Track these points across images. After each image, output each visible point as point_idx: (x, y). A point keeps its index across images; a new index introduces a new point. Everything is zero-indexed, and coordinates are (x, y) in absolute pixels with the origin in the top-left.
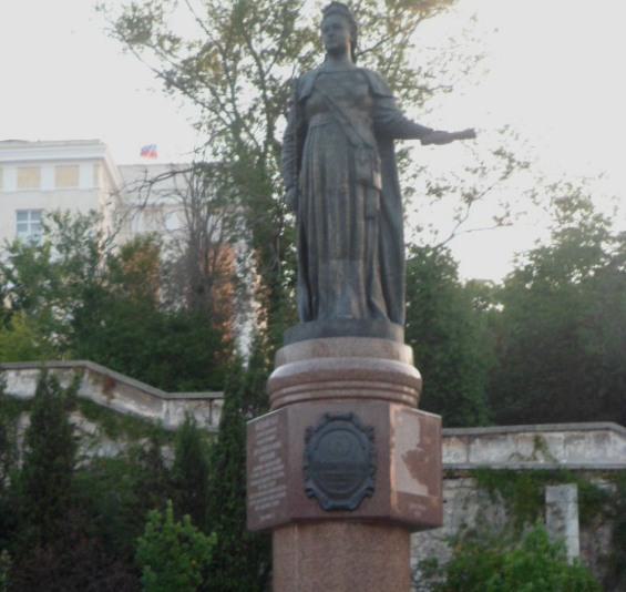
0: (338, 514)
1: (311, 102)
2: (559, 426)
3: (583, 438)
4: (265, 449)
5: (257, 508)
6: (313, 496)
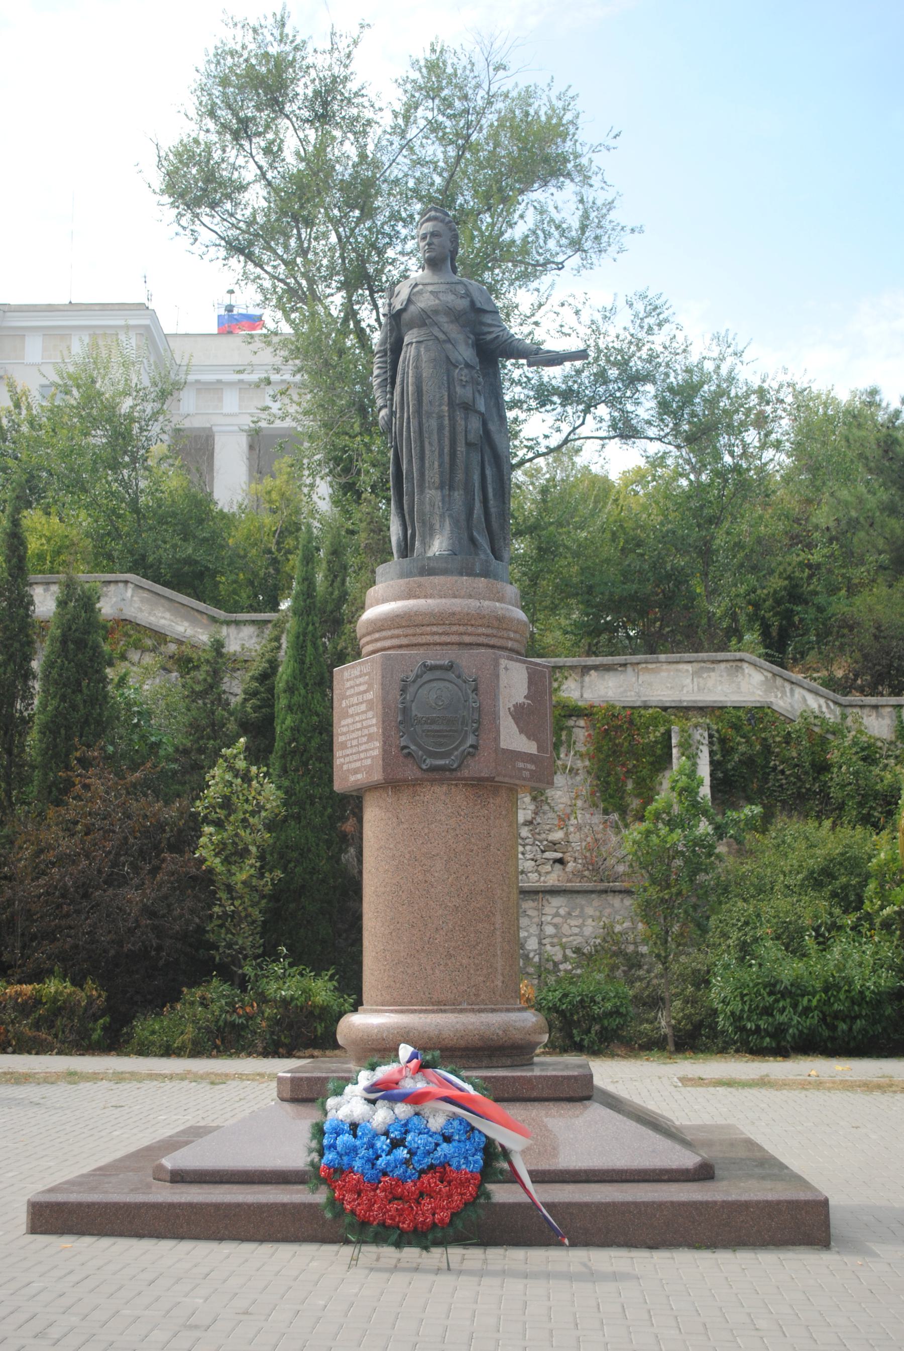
0: (440, 774)
1: (406, 316)
3: (713, 670)
4: (355, 700)
5: (345, 767)
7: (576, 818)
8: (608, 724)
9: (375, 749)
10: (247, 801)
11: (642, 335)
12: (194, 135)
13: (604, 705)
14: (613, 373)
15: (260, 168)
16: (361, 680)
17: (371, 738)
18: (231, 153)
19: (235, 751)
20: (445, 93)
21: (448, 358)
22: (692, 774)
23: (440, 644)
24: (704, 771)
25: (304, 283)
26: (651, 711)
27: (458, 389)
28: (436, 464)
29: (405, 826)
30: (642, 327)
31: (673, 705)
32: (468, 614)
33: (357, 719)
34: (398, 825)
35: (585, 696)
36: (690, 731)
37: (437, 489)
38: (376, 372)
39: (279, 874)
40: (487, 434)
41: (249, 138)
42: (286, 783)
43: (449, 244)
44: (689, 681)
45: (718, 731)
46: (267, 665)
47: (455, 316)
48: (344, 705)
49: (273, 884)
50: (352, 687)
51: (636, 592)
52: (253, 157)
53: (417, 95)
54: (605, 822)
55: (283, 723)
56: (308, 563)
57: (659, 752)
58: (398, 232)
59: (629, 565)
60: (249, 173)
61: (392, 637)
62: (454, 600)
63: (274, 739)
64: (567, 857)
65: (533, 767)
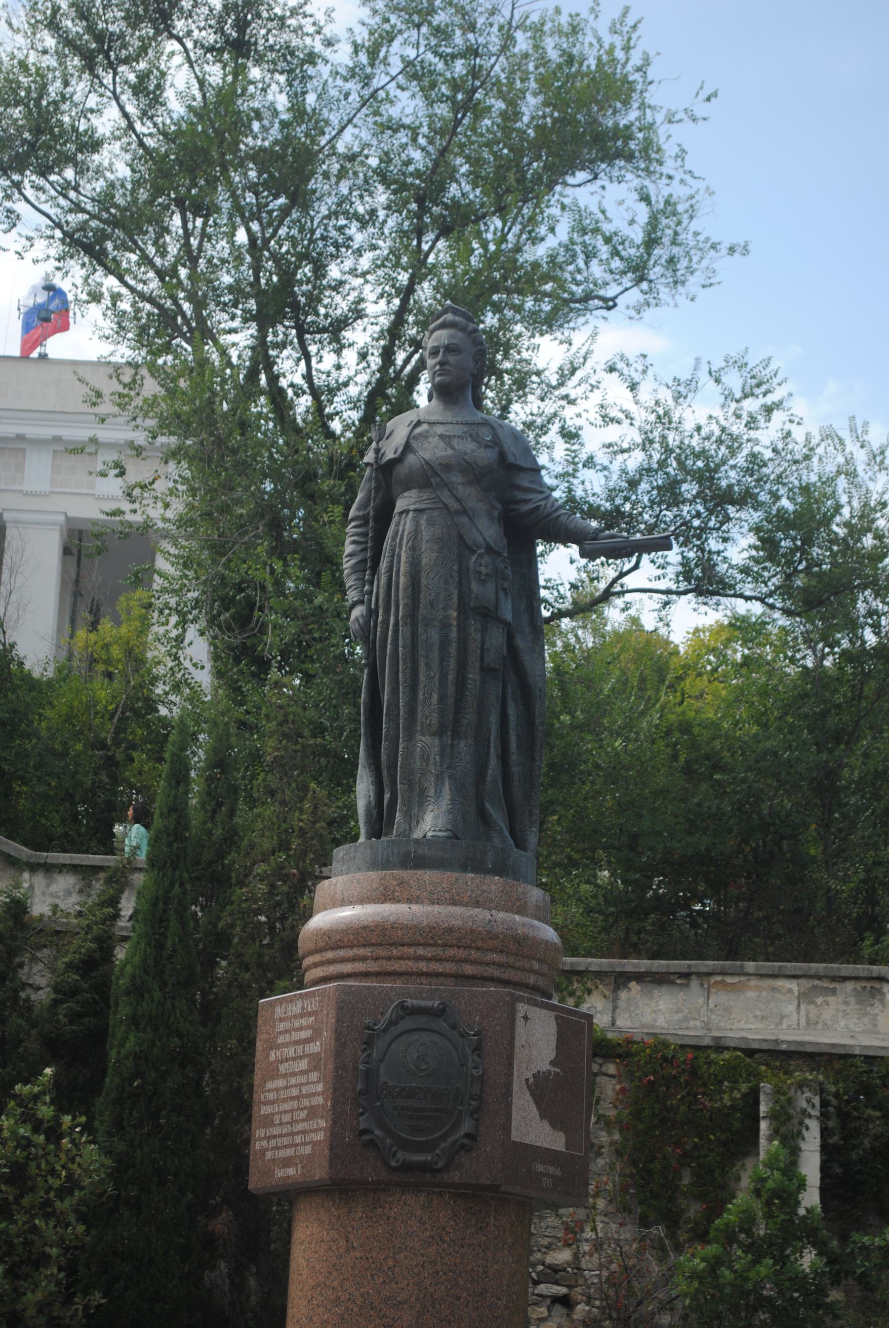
0: (416, 1178)
1: (402, 470)
2: (790, 967)
3: (834, 992)
4: (291, 1052)
5: (269, 1155)
6: (372, 1144)
7: (594, 1229)
8: (654, 1073)
9: (319, 1130)
10: (53, 1172)
11: (738, 428)
12: (20, 56)
13: (650, 1040)
14: (689, 489)
15: (126, 115)
16: (303, 1022)
17: (313, 1113)
18: (80, 87)
19: (36, 1089)
20: (440, 18)
21: (461, 537)
22: (790, 1169)
23: (427, 974)
24: (810, 1165)
25: (186, 306)
26: (726, 1055)
27: (474, 586)
28: (435, 696)
29: (358, 1254)
30: (738, 417)
31: (765, 1046)
32: (473, 931)
33: (293, 1081)
34: (347, 1251)
35: (619, 1023)
36: (791, 1093)
37: (433, 734)
38: (349, 548)
39: (97, 1298)
40: (513, 654)
41: (112, 66)
42: (120, 1146)
43: (471, 363)
44: (791, 1008)
45: (837, 1095)
46: (93, 946)
47: (472, 472)
48: (272, 1058)
49: (86, 1315)
50: (286, 1031)
51: (708, 850)
52: (117, 99)
53: (393, 19)
54: (643, 1239)
55: (122, 1045)
56: (178, 783)
57: (737, 1125)
58: (350, 238)
59: (699, 805)
60: (107, 121)
61: (353, 960)
62: (452, 909)
63: (104, 1071)
64: (577, 1294)
65: (558, 1172)
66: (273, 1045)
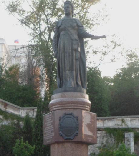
0: (68, 140)
1: (61, 28)
2: (129, 116)
3: (135, 120)
4: (48, 123)
5: (46, 139)
66: (46, 122)
